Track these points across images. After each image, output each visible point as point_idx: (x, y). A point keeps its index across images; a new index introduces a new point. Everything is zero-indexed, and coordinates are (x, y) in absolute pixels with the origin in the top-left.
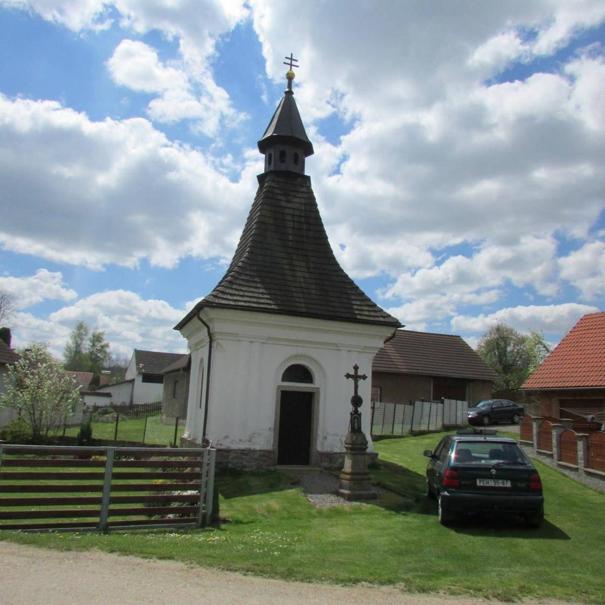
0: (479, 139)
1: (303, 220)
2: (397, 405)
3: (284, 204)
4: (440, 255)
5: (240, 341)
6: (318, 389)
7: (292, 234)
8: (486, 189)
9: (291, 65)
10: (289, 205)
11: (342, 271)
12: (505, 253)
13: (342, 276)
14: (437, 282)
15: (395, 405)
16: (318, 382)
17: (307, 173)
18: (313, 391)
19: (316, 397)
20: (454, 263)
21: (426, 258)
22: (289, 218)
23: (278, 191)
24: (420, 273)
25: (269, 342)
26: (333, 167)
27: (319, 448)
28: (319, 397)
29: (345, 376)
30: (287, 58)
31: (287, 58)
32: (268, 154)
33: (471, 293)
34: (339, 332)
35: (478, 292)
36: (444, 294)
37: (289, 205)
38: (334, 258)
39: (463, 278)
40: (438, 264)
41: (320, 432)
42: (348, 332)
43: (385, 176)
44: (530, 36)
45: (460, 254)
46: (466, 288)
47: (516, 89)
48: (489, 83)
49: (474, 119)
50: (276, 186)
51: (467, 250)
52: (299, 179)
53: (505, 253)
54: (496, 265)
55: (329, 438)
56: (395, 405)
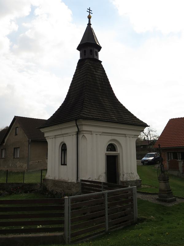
1: (103, 80)
2: (6, 182)
3: (95, 73)
6: (119, 154)
7: (99, 89)
9: (90, 13)
10: (97, 73)
11: (120, 102)
13: (122, 108)
15: (7, 182)
16: (119, 151)
17: (100, 59)
19: (118, 157)
22: (98, 79)
23: (93, 70)
27: (121, 179)
28: (119, 157)
29: (61, 2)
30: (88, 9)
31: (88, 9)
37: (97, 73)
38: (115, 97)
41: (121, 172)
50: (90, 65)
52: (98, 63)
55: (125, 175)
56: (7, 182)
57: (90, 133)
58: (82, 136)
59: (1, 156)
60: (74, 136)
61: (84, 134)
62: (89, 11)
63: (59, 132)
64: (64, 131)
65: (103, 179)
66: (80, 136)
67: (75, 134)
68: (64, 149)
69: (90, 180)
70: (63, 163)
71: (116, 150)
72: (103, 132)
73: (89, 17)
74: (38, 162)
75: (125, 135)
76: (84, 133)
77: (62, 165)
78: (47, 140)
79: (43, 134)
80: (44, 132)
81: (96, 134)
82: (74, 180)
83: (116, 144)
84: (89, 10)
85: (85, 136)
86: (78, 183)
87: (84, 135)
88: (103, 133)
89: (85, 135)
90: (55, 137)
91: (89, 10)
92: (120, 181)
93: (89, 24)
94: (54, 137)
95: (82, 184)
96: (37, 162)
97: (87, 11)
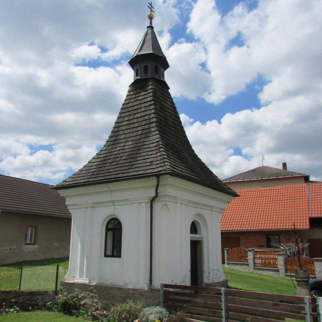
0: (69, 92)
4: (34, 149)
5: (133, 204)
6: (202, 238)
8: (68, 118)
9: (151, 10)
12: (70, 153)
14: (31, 165)
18: (200, 240)
20: (41, 154)
21: (26, 150)
24: (19, 157)
25: (189, 204)
26: (213, 91)
27: (206, 280)
30: (149, 3)
32: (136, 69)
33: (49, 172)
34: (211, 197)
35: (54, 173)
36: (33, 171)
39: (46, 163)
40: (31, 154)
42: (212, 197)
43: (10, 98)
44: (104, 50)
45: (47, 150)
46: (48, 169)
47: (90, 72)
48: (77, 65)
49: (68, 80)
51: (50, 148)
53: (70, 153)
54: (65, 159)
57: (174, 201)
58: (164, 205)
59: (26, 239)
60: (143, 205)
61: (168, 203)
62: (150, 6)
63: (106, 197)
64: (117, 196)
65: (188, 283)
66: (157, 206)
67: (147, 201)
68: (114, 229)
69: (173, 283)
70: (109, 253)
71: (198, 232)
72: (94, 202)
73: (151, 18)
74: (10, 249)
75: (211, 207)
76: (167, 199)
77: (106, 256)
78: (69, 210)
79: (63, 199)
80: (65, 196)
81: (181, 204)
82: (146, 287)
83: (201, 223)
84: (151, 5)
85: (167, 206)
86: (152, 290)
87: (166, 204)
88: (190, 202)
89: (168, 203)
90: (94, 205)
91: (151, 5)
92: (204, 284)
93: (151, 27)
94: (91, 205)
95: (166, 293)
96: (9, 249)
97: (148, 6)
